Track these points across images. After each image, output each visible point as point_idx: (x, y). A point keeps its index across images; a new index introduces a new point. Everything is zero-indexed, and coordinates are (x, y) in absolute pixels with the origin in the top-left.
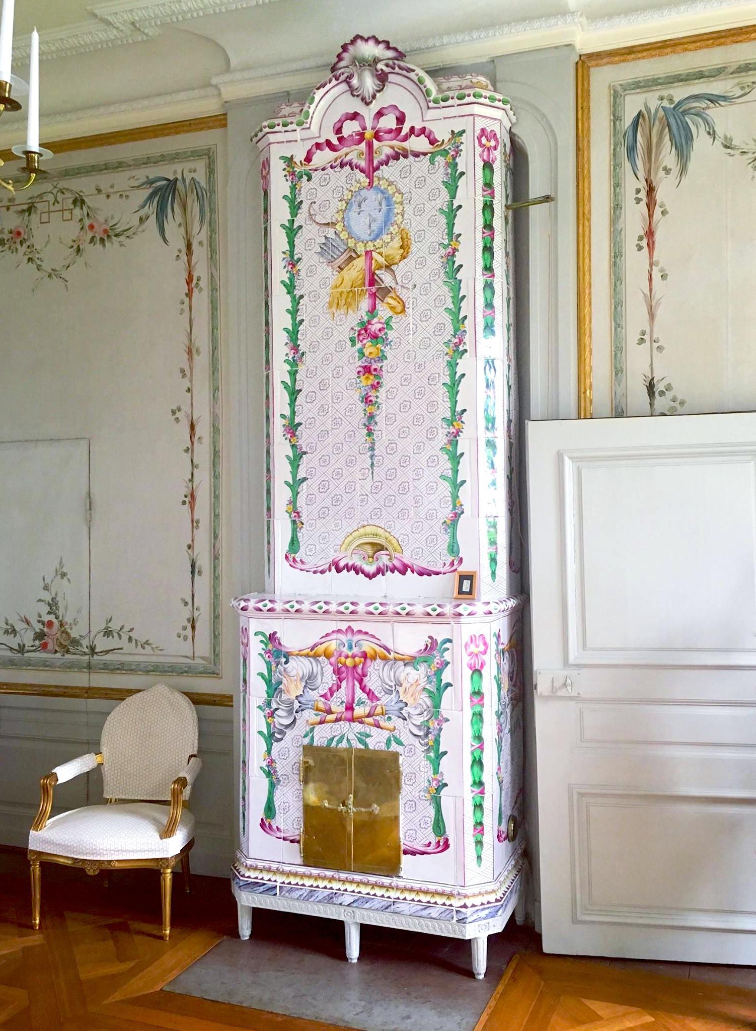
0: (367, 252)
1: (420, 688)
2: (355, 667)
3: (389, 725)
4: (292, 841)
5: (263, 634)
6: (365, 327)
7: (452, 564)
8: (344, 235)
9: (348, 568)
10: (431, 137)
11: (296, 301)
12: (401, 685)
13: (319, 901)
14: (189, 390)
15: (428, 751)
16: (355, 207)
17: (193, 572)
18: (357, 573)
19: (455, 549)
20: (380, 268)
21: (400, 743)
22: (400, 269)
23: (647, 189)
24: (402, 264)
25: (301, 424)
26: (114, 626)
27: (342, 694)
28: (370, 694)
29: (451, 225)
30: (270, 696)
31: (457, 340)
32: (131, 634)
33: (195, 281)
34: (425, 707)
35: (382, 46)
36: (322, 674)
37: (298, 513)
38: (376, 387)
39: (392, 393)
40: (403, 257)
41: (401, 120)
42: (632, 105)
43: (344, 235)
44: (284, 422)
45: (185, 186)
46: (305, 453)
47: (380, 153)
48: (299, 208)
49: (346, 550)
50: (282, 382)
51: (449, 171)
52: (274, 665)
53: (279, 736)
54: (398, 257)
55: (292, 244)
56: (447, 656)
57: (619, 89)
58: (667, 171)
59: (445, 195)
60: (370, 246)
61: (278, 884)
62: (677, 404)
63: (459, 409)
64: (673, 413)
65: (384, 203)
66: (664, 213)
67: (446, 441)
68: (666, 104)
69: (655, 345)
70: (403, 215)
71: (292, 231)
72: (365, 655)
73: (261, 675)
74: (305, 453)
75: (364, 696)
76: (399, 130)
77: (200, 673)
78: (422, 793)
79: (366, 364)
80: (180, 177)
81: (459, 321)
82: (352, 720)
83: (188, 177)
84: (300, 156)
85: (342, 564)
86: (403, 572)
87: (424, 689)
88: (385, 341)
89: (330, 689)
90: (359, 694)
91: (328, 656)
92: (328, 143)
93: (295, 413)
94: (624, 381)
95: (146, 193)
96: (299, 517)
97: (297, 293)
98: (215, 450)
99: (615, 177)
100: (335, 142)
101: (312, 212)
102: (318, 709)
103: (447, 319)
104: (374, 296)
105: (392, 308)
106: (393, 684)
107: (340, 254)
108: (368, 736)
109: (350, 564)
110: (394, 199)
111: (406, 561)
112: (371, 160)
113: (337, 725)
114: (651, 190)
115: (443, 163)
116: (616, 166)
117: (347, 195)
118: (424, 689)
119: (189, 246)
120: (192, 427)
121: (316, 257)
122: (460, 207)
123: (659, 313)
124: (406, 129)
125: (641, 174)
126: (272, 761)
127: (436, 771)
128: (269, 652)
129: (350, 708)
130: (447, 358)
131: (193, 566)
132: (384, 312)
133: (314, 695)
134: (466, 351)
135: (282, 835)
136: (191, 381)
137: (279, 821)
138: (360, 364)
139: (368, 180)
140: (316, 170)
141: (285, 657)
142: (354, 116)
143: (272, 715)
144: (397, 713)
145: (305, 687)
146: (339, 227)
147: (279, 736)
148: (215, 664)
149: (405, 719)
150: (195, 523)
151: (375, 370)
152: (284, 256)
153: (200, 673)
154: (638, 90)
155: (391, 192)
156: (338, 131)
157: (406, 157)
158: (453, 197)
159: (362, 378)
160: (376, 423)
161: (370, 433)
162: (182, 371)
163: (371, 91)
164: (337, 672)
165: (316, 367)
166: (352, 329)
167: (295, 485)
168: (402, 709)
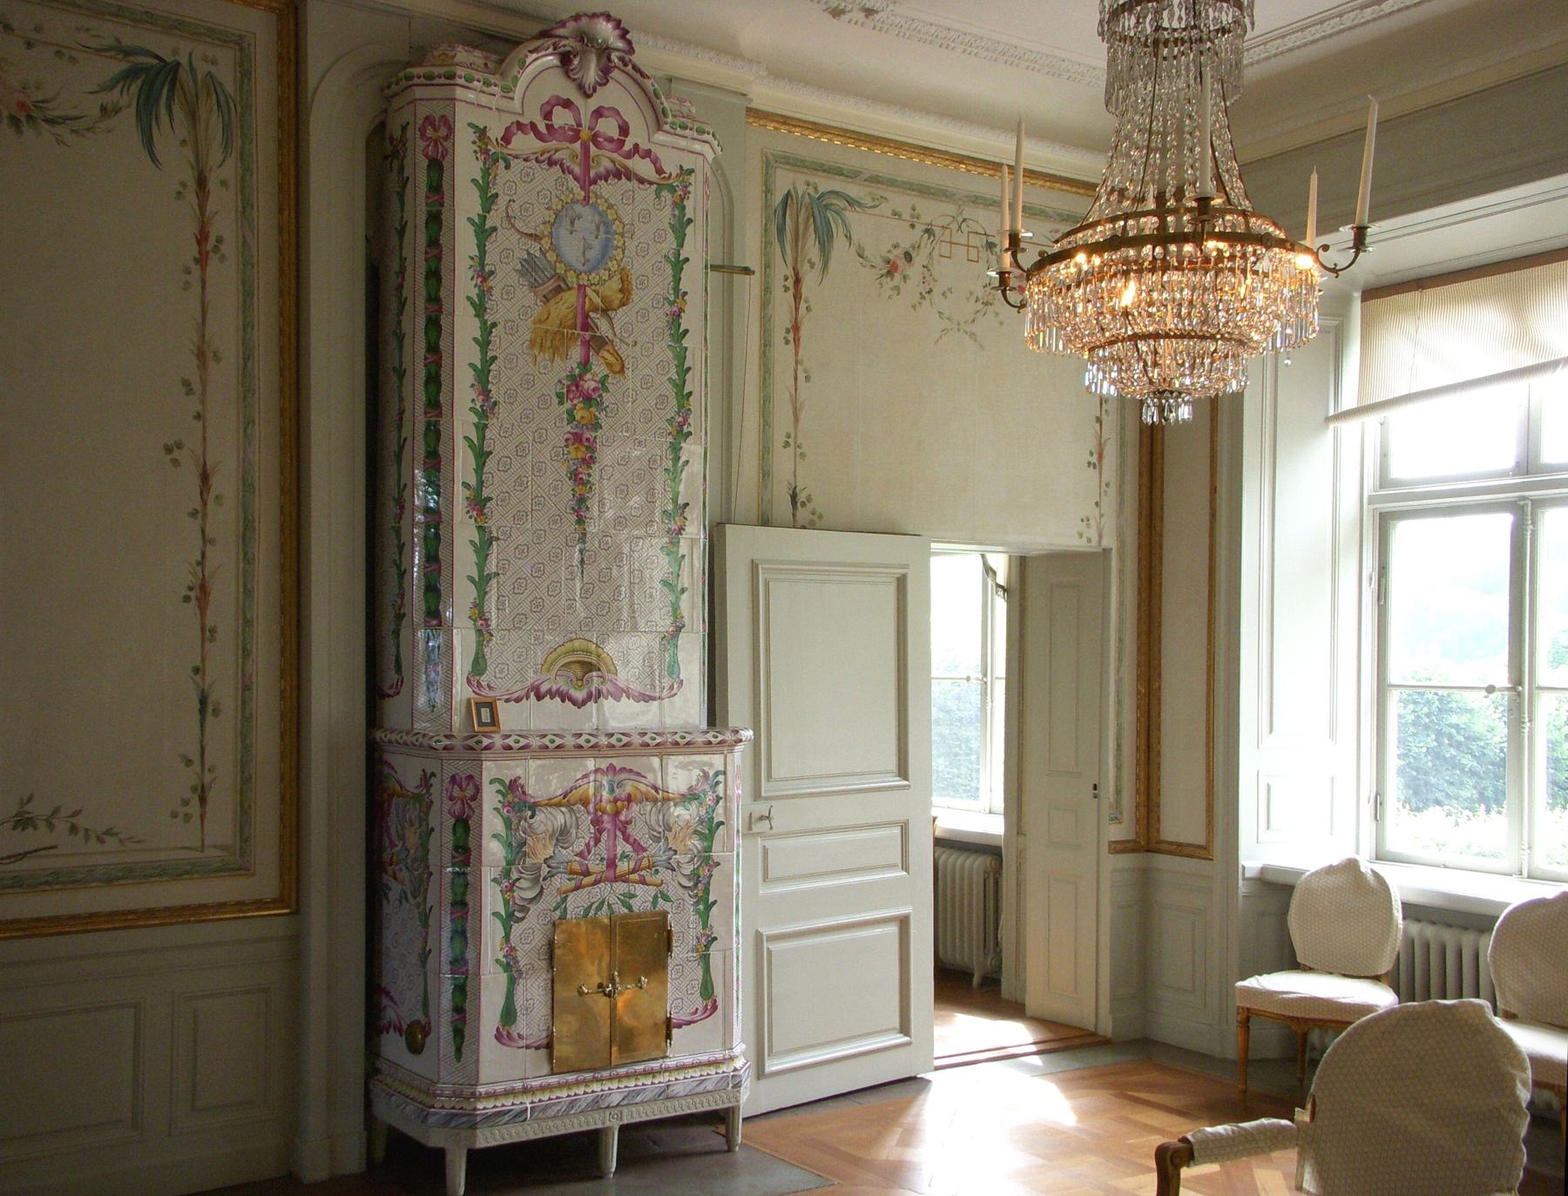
0: (580, 286)
3: (657, 879)
4: (537, 1048)
5: (501, 781)
6: (575, 381)
7: (672, 687)
8: (551, 256)
9: (552, 694)
11: (488, 329)
14: (198, 417)
15: (697, 903)
16: (566, 223)
17: (202, 711)
20: (596, 310)
21: (667, 899)
22: (620, 316)
26: (38, 809)
28: (638, 847)
29: (677, 280)
32: (74, 820)
33: (211, 243)
35: (617, 32)
38: (589, 462)
40: (623, 304)
41: (624, 130)
42: (785, 181)
43: (551, 256)
44: (467, 493)
45: (195, 81)
50: (466, 438)
54: (616, 303)
58: (812, 265)
59: (670, 242)
60: (584, 280)
64: (810, 526)
65: (602, 228)
66: (808, 309)
68: (811, 190)
71: (483, 233)
75: (628, 848)
76: (622, 143)
80: (184, 61)
81: (684, 397)
82: (616, 879)
83: (202, 68)
84: (496, 133)
85: (544, 688)
87: (696, 832)
90: (622, 847)
92: (533, 126)
95: (117, 67)
97: (490, 318)
98: (245, 518)
100: (542, 127)
102: (572, 872)
103: (670, 391)
104: (587, 344)
105: (609, 365)
107: (546, 279)
108: (633, 896)
113: (596, 889)
114: (797, 281)
115: (669, 202)
116: (767, 244)
117: (557, 205)
119: (202, 182)
120: (205, 478)
121: (515, 276)
122: (687, 260)
123: (803, 415)
124: (628, 146)
126: (513, 949)
127: (705, 925)
129: (612, 864)
131: (203, 702)
132: (598, 368)
133: (566, 854)
134: (690, 434)
135: (522, 1043)
136: (203, 402)
137: (521, 1026)
140: (516, 157)
142: (567, 104)
143: (511, 888)
146: (546, 243)
148: (242, 856)
150: (208, 633)
156: (548, 116)
157: (629, 179)
158: (681, 245)
159: (571, 448)
161: (580, 521)
164: (596, 822)
167: (482, 582)
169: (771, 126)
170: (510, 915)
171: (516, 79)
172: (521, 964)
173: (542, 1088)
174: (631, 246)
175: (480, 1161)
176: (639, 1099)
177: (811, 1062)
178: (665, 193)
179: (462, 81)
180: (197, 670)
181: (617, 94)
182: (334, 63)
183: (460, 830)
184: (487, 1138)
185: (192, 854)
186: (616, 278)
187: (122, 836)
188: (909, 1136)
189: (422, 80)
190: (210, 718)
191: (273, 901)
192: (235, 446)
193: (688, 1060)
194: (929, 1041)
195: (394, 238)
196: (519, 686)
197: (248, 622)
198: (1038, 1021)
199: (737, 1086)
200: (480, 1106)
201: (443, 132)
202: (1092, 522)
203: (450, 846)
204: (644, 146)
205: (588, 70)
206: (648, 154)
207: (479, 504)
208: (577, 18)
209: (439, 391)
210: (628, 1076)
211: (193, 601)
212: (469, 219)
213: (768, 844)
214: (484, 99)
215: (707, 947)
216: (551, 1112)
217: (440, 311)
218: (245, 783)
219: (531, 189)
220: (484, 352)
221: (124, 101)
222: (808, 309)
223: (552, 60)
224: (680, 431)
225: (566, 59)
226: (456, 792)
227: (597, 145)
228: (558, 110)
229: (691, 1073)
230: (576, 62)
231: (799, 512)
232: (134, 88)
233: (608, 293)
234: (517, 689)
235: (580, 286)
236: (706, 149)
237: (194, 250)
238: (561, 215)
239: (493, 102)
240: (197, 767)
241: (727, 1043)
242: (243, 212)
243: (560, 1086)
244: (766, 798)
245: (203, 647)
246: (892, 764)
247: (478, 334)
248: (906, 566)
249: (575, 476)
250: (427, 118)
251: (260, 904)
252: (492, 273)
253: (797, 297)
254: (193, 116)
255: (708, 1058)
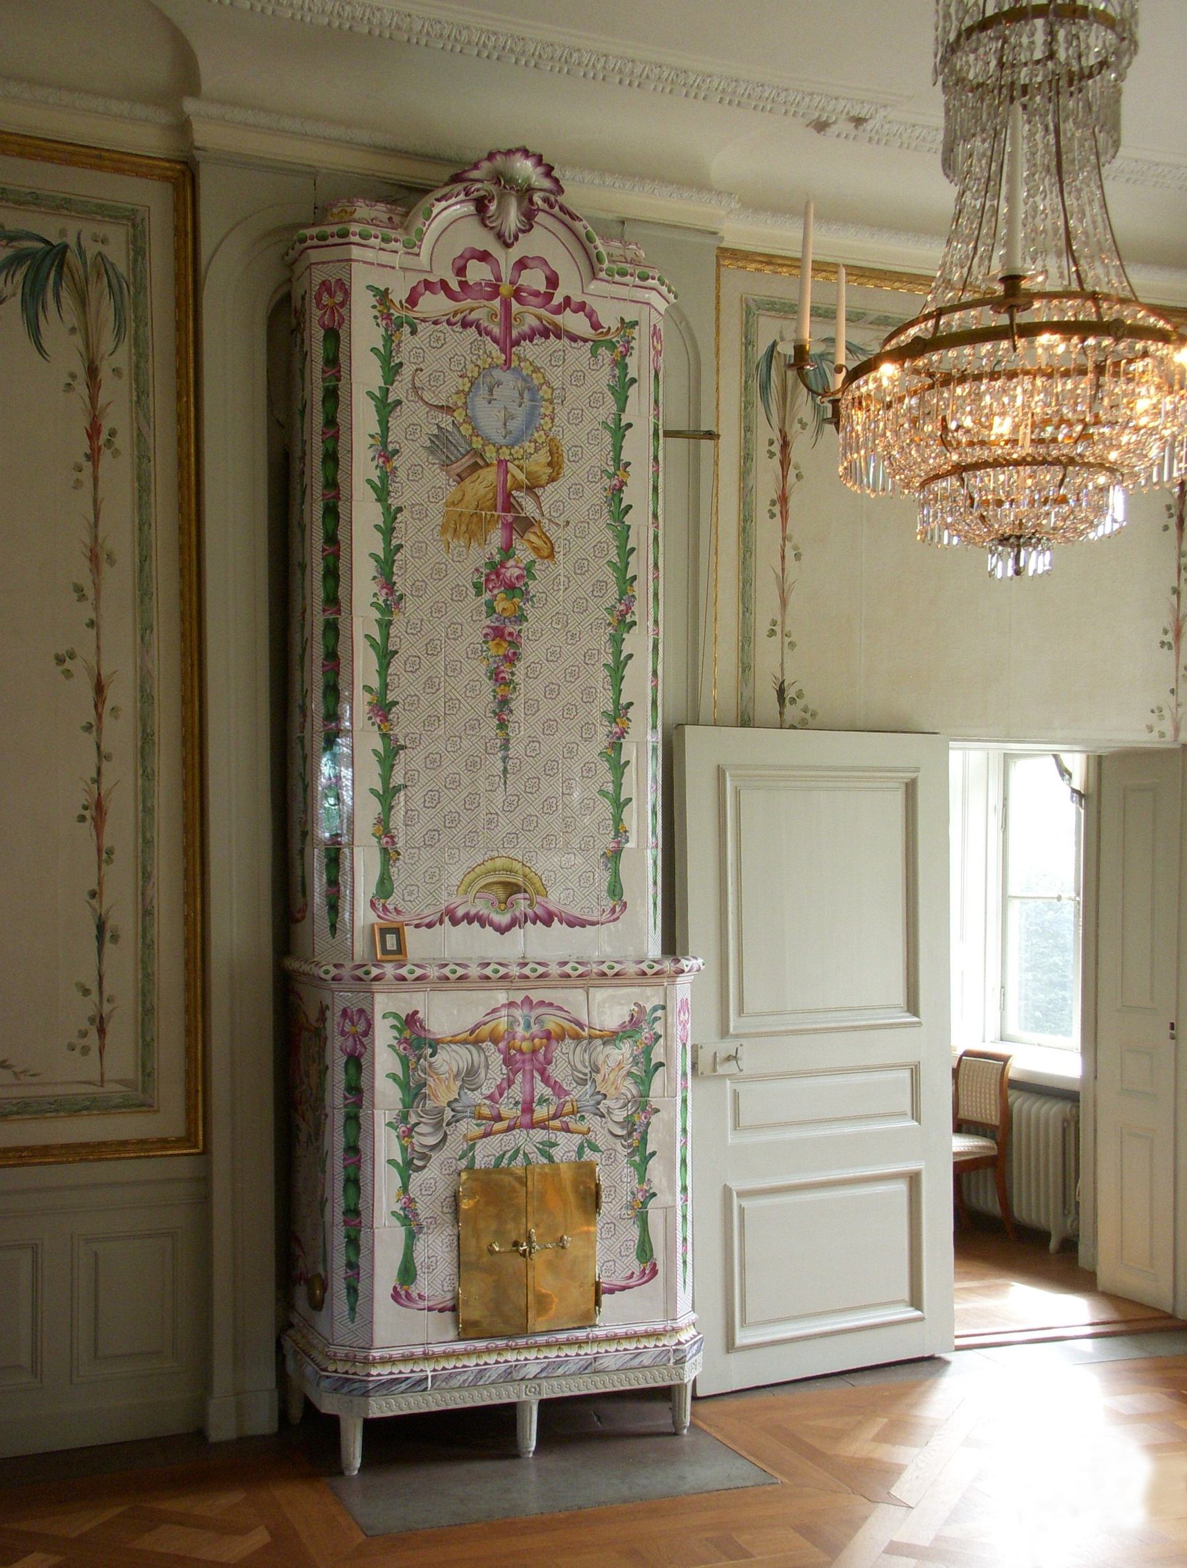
0: (500, 462)
1: (623, 1072)
2: (534, 1051)
3: (583, 1126)
4: (441, 1310)
5: (396, 1016)
6: (495, 569)
7: (613, 911)
8: (466, 430)
9: (469, 919)
10: (594, 319)
11: (391, 515)
12: (598, 1071)
13: (492, 1383)
14: (91, 624)
15: (631, 1155)
16: (483, 391)
18: (483, 926)
19: (617, 891)
20: (519, 488)
21: (595, 1149)
22: (549, 494)
23: (781, 442)
24: (549, 488)
25: (397, 703)
27: (517, 1091)
29: (618, 449)
30: (407, 1105)
31: (622, 607)
33: (104, 436)
34: (629, 1096)
35: (540, 170)
36: (487, 1067)
37: (392, 837)
38: (512, 659)
39: (534, 671)
40: (552, 479)
41: (553, 281)
44: (368, 697)
45: (84, 264)
46: (403, 747)
47: (522, 322)
48: (397, 373)
49: (466, 892)
50: (367, 636)
51: (617, 372)
52: (413, 1060)
53: (420, 1163)
54: (545, 478)
55: (385, 428)
56: (658, 1028)
57: (752, 305)
58: (804, 426)
59: (610, 404)
60: (505, 454)
61: (430, 1374)
62: (808, 716)
63: (624, 701)
64: (803, 725)
65: (526, 395)
66: (799, 476)
67: (606, 744)
69: (787, 640)
70: (553, 420)
71: (385, 407)
72: (548, 1035)
73: (393, 1077)
74: (403, 747)
75: (548, 1091)
76: (549, 297)
77: (117, 1107)
78: (624, 1211)
79: (497, 624)
80: (72, 243)
81: (626, 582)
82: (532, 1125)
83: (92, 249)
84: (399, 295)
85: (460, 912)
86: (548, 922)
87: (629, 1074)
88: (524, 594)
89: (499, 1087)
90: (541, 1089)
91: (495, 1041)
92: (444, 284)
93: (387, 685)
94: (751, 681)
96: (394, 843)
97: (394, 502)
98: (144, 731)
99: (746, 417)
100: (454, 285)
101: (418, 384)
103: (610, 577)
104: (509, 527)
105: (536, 549)
106: (587, 1071)
107: (460, 455)
109: (473, 912)
110: (541, 393)
111: (552, 908)
112: (508, 327)
113: (509, 1137)
114: (785, 445)
115: (607, 360)
116: (747, 405)
117: (472, 372)
118: (629, 1074)
119: (92, 371)
120: (99, 689)
121: (424, 454)
122: (629, 425)
123: (792, 599)
124: (558, 299)
125: (775, 420)
127: (642, 1179)
128: (406, 1041)
129: (528, 1109)
130: (610, 630)
131: (101, 927)
132: (523, 552)
133: (476, 1097)
134: (634, 623)
135: (422, 1304)
136: (96, 608)
137: (423, 1285)
138: (488, 622)
139: (503, 357)
140: (424, 320)
141: (431, 1046)
142: (484, 256)
143: (409, 1133)
144: (593, 1109)
145: (461, 1087)
146: (459, 416)
147: (420, 1163)
148: (144, 1091)
149: (602, 1116)
150: (104, 855)
151: (511, 634)
152: (371, 441)
153: (117, 1107)
154: (773, 313)
155: (536, 382)
156: (461, 271)
157: (559, 337)
160: (511, 711)
161: (502, 725)
162: (79, 589)
163: (513, 229)
164: (508, 1061)
165: (422, 620)
166: (477, 570)
168: (599, 1103)
169: (752, 267)
170: (409, 1164)
171: (421, 235)
172: (422, 1216)
173: (447, 1356)
174: (561, 413)
175: (373, 1428)
176: (560, 1371)
177: (796, 1335)
178: (603, 351)
179: (357, 239)
180: (93, 894)
181: (545, 242)
182: (227, 234)
183: (352, 1070)
184: (381, 1407)
185: (90, 1089)
186: (544, 451)
187: (18, 1070)
188: (900, 1429)
189: (315, 242)
190: (108, 946)
191: (179, 1140)
192: (133, 652)
193: (620, 1331)
194: (949, 1317)
195: (298, 417)
196: (431, 910)
197: (148, 843)
198: (1112, 1298)
199: (680, 1361)
200: (374, 1372)
201: (339, 298)
202: (1166, 712)
203: (342, 1085)
204: (577, 298)
205: (508, 213)
206: (582, 307)
207: (383, 709)
208: (491, 156)
209: (337, 586)
210: (548, 1345)
211: (89, 820)
212: (369, 393)
213: (740, 1088)
214: (385, 258)
215: (644, 1204)
216: (455, 1383)
217: (337, 497)
218: (147, 1012)
219: (442, 356)
220: (387, 542)
221: (8, 290)
222: (799, 476)
223: (470, 208)
224: (622, 621)
225: (481, 205)
226: (348, 1027)
227: (520, 300)
228: (473, 265)
229: (626, 1345)
230: (493, 207)
231: (788, 709)
232: (19, 277)
233: (534, 468)
234: (430, 913)
235: (500, 462)
236: (653, 297)
237: (85, 446)
238: (478, 381)
239: (396, 260)
240: (95, 996)
241: (670, 1309)
242: (138, 402)
243: (467, 1354)
244: (737, 1036)
245: (99, 868)
246: (900, 997)
247: (380, 521)
248: (917, 770)
249: (496, 676)
250: (323, 283)
251: (164, 1143)
252: (396, 452)
253: (785, 463)
254: (82, 301)
255: (671, 1323)
